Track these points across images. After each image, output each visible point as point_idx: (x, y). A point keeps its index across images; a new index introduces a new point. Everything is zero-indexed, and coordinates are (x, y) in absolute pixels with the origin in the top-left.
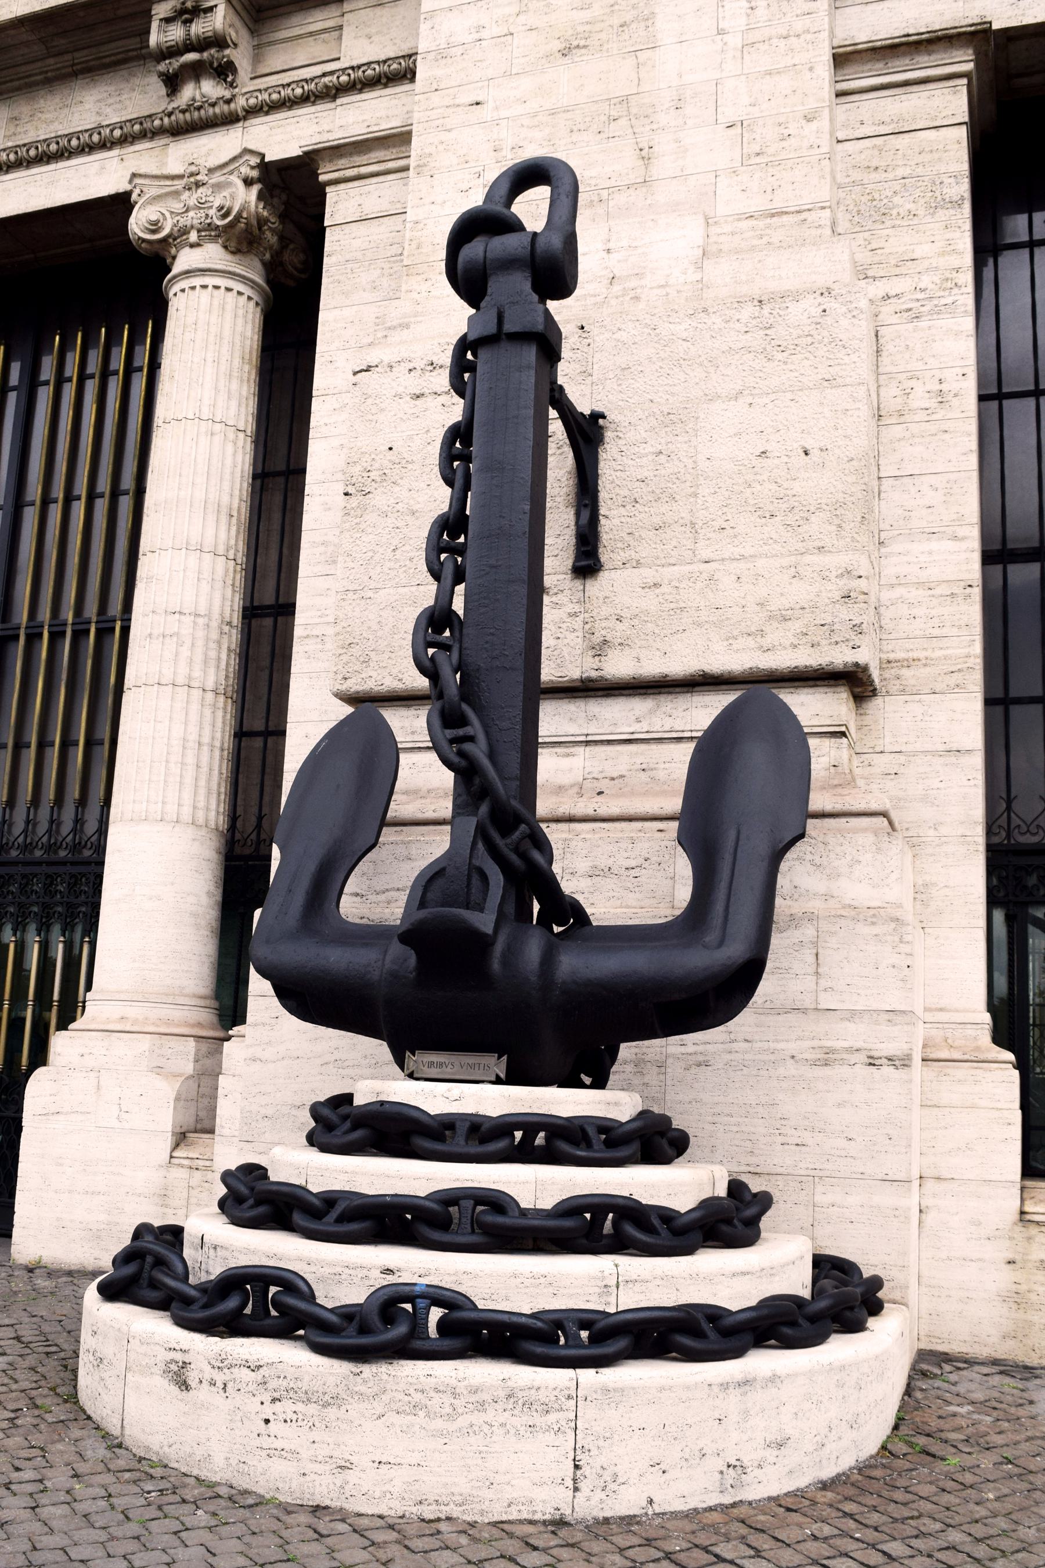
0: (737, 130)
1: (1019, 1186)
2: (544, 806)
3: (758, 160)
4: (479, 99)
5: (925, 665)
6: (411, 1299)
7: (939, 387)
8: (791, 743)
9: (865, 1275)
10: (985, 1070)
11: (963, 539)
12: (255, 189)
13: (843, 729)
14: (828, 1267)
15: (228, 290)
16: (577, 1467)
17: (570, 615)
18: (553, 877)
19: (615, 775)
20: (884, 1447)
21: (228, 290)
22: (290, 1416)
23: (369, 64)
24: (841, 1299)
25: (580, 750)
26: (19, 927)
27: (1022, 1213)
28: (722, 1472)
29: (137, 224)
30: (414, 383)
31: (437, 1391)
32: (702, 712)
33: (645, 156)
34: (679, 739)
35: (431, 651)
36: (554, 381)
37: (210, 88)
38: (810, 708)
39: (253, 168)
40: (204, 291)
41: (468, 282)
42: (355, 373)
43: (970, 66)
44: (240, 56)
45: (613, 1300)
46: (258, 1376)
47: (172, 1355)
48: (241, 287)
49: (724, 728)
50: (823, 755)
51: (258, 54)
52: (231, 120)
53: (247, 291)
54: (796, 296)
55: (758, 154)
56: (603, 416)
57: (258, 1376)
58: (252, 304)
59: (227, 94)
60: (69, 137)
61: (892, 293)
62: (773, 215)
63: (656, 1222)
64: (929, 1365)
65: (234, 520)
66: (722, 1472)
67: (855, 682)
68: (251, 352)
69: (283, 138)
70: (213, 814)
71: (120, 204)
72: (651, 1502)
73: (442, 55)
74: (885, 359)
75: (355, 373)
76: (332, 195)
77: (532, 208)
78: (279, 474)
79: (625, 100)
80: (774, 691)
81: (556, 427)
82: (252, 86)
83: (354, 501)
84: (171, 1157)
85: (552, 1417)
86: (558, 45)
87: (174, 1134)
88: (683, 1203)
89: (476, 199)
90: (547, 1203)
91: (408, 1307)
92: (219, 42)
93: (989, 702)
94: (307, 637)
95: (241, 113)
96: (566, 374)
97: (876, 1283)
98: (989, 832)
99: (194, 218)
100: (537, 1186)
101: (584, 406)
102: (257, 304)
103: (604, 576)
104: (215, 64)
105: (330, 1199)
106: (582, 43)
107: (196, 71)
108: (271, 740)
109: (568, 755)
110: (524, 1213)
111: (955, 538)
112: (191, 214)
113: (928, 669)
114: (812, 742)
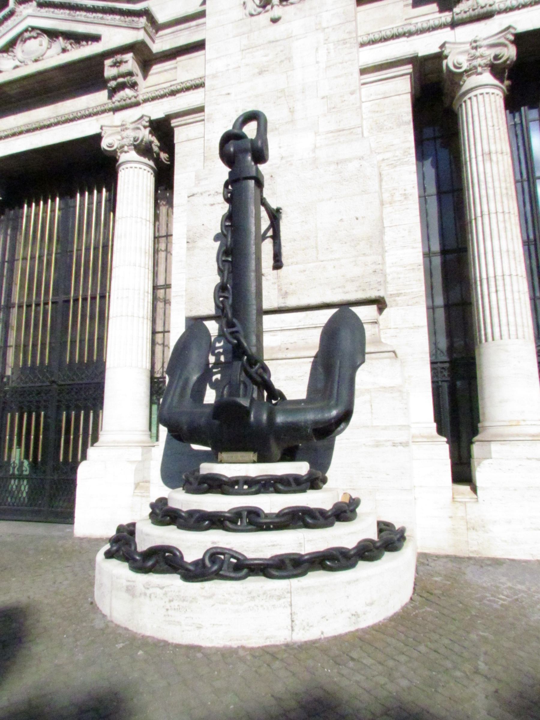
0: (325, 100)
1: (451, 488)
2: (265, 357)
3: (333, 110)
4: (229, 92)
5: (405, 295)
6: (223, 554)
7: (404, 192)
8: (358, 327)
9: (397, 528)
10: (436, 445)
11: (416, 248)
12: (148, 129)
13: (376, 321)
14: (383, 527)
15: (140, 168)
16: (293, 621)
17: (273, 283)
18: (271, 382)
19: (292, 342)
20: (411, 599)
21: (140, 168)
22: (176, 607)
23: (187, 81)
24: (389, 540)
25: (279, 333)
26: (68, 409)
27: (453, 498)
28: (350, 618)
29: (104, 144)
30: (211, 200)
31: (235, 593)
32: (327, 315)
33: (292, 111)
34: (163, 352)
35: (221, 299)
36: (262, 196)
37: (128, 92)
38: (361, 312)
39: (147, 122)
40: (131, 169)
41: (228, 158)
42: (189, 197)
43: (411, 70)
44: (139, 78)
45: (303, 549)
46: (163, 591)
47: (129, 584)
48: (145, 167)
49: (332, 321)
50: (369, 331)
51: (145, 77)
52: (137, 104)
53: (148, 169)
54: (350, 160)
55: (334, 108)
56: (281, 209)
57: (163, 591)
58: (149, 174)
59: (135, 94)
60: (77, 112)
61: (385, 158)
62: (340, 131)
63: (318, 514)
64: (423, 559)
65: (147, 254)
66: (350, 618)
67: (380, 303)
68: (150, 192)
69: (157, 111)
70: (144, 363)
71: (98, 137)
72: (322, 633)
73: (214, 76)
74: (384, 183)
75: (189, 197)
76: (177, 131)
77: (250, 130)
78: (164, 237)
79: (283, 91)
80: (350, 308)
81: (264, 214)
82: (144, 91)
83: (190, 245)
84: (134, 493)
85: (282, 601)
86: (257, 70)
87: (135, 484)
88: (328, 506)
89: (230, 127)
90: (276, 510)
91: (222, 557)
92: (130, 74)
93: (428, 308)
94: (177, 296)
95: (141, 102)
96: (267, 193)
97: (402, 531)
98: (431, 356)
99: (126, 141)
100: (271, 503)
101: (274, 205)
102: (152, 174)
103: (284, 268)
104: (130, 83)
105: (191, 513)
106: (266, 69)
107: (122, 87)
108: (166, 334)
109: (274, 335)
110: (267, 516)
111: (413, 248)
112: (125, 140)
113: (405, 297)
114: (365, 326)
